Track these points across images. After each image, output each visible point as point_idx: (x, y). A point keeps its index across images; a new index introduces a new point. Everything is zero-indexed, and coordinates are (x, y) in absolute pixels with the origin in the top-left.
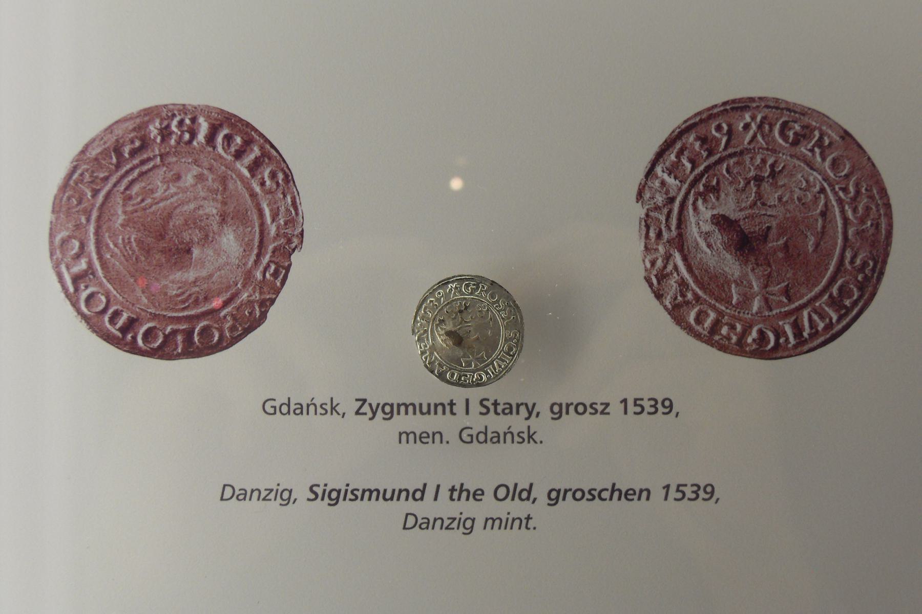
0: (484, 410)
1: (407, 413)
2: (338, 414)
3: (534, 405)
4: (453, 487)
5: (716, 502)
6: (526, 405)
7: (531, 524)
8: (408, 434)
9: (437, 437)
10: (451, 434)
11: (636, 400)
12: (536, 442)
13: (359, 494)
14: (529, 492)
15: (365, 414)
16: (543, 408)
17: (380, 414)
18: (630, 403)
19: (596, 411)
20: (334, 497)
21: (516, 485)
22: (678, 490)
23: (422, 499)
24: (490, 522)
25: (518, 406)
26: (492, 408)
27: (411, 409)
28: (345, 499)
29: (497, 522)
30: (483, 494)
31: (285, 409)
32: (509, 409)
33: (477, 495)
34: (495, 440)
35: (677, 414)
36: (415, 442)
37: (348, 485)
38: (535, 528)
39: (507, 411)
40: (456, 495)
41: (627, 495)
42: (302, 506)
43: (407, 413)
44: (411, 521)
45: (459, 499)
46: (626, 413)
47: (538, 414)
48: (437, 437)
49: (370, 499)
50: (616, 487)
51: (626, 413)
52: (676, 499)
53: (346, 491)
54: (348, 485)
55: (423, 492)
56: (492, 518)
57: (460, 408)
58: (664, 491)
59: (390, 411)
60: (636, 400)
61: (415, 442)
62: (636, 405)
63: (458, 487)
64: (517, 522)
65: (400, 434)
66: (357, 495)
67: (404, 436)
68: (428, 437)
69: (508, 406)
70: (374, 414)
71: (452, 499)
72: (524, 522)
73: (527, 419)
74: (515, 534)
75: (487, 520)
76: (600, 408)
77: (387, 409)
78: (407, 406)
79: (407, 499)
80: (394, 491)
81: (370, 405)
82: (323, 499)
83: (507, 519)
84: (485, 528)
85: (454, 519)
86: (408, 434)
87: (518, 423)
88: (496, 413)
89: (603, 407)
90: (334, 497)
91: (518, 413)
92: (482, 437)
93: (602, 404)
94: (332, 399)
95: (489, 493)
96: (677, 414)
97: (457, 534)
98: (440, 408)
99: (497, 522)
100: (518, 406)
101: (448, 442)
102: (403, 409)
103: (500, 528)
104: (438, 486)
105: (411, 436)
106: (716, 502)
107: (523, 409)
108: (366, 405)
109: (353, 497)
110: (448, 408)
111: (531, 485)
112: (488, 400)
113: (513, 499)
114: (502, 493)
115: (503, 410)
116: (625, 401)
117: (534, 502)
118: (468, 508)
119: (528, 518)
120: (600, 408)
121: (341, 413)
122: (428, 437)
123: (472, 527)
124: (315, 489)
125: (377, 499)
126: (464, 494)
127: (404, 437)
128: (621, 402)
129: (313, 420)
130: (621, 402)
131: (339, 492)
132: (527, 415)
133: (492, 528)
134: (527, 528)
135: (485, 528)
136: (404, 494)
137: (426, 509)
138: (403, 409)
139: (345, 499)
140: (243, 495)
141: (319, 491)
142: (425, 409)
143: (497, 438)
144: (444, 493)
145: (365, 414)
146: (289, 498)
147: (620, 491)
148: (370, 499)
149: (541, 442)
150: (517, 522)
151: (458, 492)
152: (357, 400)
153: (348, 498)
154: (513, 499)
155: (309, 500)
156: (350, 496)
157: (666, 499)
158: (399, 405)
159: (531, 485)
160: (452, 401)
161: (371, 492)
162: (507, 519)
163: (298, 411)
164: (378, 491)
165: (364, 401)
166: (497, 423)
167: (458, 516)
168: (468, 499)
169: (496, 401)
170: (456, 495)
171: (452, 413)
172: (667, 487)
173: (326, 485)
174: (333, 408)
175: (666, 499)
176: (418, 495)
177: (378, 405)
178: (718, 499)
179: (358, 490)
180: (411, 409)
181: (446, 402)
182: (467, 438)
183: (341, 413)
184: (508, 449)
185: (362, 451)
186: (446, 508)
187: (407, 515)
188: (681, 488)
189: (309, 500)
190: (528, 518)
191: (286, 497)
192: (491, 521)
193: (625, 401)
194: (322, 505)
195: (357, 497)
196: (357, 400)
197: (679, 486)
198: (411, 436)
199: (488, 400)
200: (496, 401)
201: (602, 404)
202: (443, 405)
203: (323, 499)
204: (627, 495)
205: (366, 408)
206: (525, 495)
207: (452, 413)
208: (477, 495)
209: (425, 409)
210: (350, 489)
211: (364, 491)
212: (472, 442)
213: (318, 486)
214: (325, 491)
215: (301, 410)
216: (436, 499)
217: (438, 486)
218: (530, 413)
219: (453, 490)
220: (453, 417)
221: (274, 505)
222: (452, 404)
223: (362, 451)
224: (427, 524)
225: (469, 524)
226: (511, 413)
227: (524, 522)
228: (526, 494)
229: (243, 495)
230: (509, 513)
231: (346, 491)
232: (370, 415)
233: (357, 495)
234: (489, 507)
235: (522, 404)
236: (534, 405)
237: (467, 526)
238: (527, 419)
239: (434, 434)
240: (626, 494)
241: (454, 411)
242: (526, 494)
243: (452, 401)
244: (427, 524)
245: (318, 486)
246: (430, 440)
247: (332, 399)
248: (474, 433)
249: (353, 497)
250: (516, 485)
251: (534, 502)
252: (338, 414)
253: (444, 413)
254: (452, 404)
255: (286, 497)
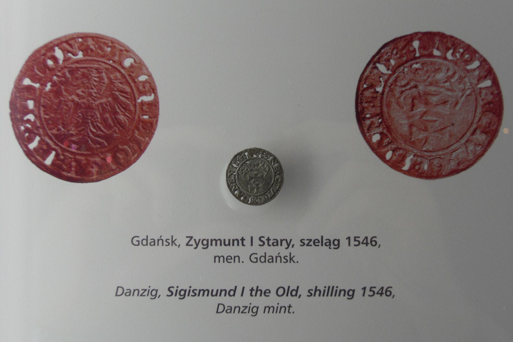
0: (262, 243)
1: (216, 245)
2: (176, 245)
3: (291, 240)
4: (252, 288)
5: (393, 297)
6: (286, 240)
7: (291, 310)
8: (219, 258)
9: (237, 259)
10: (244, 257)
11: (355, 238)
12: (294, 262)
13: (197, 292)
14: (297, 291)
15: (192, 245)
16: (296, 242)
17: (200, 245)
18: (352, 240)
19: (304, 244)
20: (183, 294)
21: (289, 287)
22: (371, 290)
23: (234, 295)
24: (267, 309)
25: (281, 241)
26: (266, 242)
27: (219, 242)
28: (188, 295)
29: (272, 309)
30: (270, 292)
31: (145, 242)
32: (276, 243)
33: (266, 293)
34: (152, 244)
35: (380, 246)
36: (224, 262)
37: (190, 287)
38: (293, 312)
39: (275, 244)
40: (254, 293)
41: (331, 291)
42: (165, 301)
43: (216, 245)
44: (221, 308)
45: (256, 295)
46: (349, 245)
47: (293, 245)
48: (237, 259)
49: (203, 295)
50: (259, 289)
51: (349, 245)
52: (369, 296)
53: (190, 291)
54: (190, 287)
55: (235, 291)
56: (269, 307)
57: (247, 242)
58: (363, 291)
59: (207, 244)
60: (355, 238)
61: (224, 262)
62: (355, 240)
63: (255, 288)
64: (283, 309)
65: (215, 257)
66: (196, 293)
67: (217, 258)
68: (232, 259)
69: (275, 241)
70: (197, 245)
71: (251, 295)
72: (287, 309)
73: (287, 248)
74: (282, 316)
75: (265, 308)
76: (306, 242)
77: (205, 242)
78: (216, 241)
79: (225, 295)
80: (217, 290)
81: (195, 240)
82: (176, 295)
83: (278, 307)
84: (264, 312)
85: (246, 307)
86: (219, 258)
87: (282, 250)
88: (269, 245)
89: (308, 241)
90: (183, 294)
91: (281, 245)
92: (263, 259)
93: (307, 240)
94: (172, 236)
95: (273, 292)
96: (380, 246)
97: (248, 316)
98: (236, 242)
99: (272, 309)
100: (281, 241)
101: (243, 262)
102: (214, 242)
103: (273, 312)
104: (244, 288)
105: (222, 259)
106: (393, 297)
107: (284, 243)
108: (193, 240)
109: (194, 294)
110: (240, 242)
111: (298, 287)
112: (264, 237)
113: (287, 295)
114: (281, 292)
115: (273, 243)
116: (349, 238)
117: (299, 297)
118: (260, 301)
119: (290, 307)
120: (306, 242)
121: (178, 245)
122: (232, 259)
123: (257, 312)
124: (171, 289)
125: (208, 295)
126: (259, 292)
127: (217, 259)
128: (347, 239)
129: (160, 249)
130: (347, 239)
131: (185, 291)
132: (287, 246)
133: (269, 312)
134: (289, 312)
135: (264, 312)
136: (223, 293)
137: (228, 301)
138: (214, 242)
139: (188, 295)
140: (129, 293)
141: (174, 290)
142: (227, 243)
143: (272, 260)
144: (247, 292)
145: (192, 245)
146: (156, 295)
147: (261, 291)
148: (203, 295)
149: (297, 262)
150: (283, 309)
151: (255, 291)
152: (187, 237)
153: (190, 295)
154: (287, 295)
155: (168, 296)
156: (191, 293)
157: (364, 295)
158: (212, 241)
159: (298, 287)
160: (243, 238)
161: (204, 291)
162: (278, 307)
163: (270, 261)
164: (208, 291)
165: (191, 238)
166: (272, 251)
167: (248, 305)
168: (261, 295)
169: (268, 238)
170: (254, 293)
171: (243, 245)
172: (364, 289)
173: (178, 287)
174: (173, 242)
175: (364, 295)
176: (232, 293)
177: (200, 240)
178: (394, 296)
179: (196, 290)
180: (219, 242)
181: (239, 238)
182: (254, 259)
183: (178, 245)
184: (277, 266)
185: (200, 269)
186: (247, 300)
187: (219, 305)
188: (373, 289)
189: (168, 296)
190: (290, 307)
191: (154, 294)
192: (268, 308)
193: (349, 238)
194: (175, 299)
195: (196, 294)
196: (187, 237)
197: (371, 288)
198: (222, 259)
199: (264, 237)
200: (268, 238)
201: (307, 240)
202: (238, 240)
203: (176, 295)
204: (331, 291)
205: (192, 242)
206: (294, 293)
207: (243, 245)
208: (266, 293)
209: (227, 243)
210: (192, 289)
211: (200, 291)
212: (139, 245)
213: (173, 287)
214: (177, 290)
215: (154, 243)
216: (242, 295)
217: (244, 288)
218: (289, 245)
219: (252, 290)
220: (244, 247)
221: (147, 299)
222: (243, 239)
223: (200, 269)
224: (230, 310)
225: (255, 310)
226: (277, 245)
227: (287, 309)
228: (294, 292)
229: (129, 293)
230: (278, 304)
231: (190, 291)
232: (195, 246)
233: (196, 293)
234: (273, 300)
235: (284, 240)
236: (291, 240)
237: (254, 311)
238: (287, 248)
239: (235, 257)
240: (265, 292)
241: (244, 244)
242: (294, 292)
243: (243, 238)
244: (230, 310)
245: (173, 287)
246: (232, 261)
247: (172, 236)
248: (140, 240)
249: (194, 294)
250: (289, 287)
251: (299, 297)
252: (176, 245)
253: (238, 245)
254: (243, 239)
255: (154, 294)
